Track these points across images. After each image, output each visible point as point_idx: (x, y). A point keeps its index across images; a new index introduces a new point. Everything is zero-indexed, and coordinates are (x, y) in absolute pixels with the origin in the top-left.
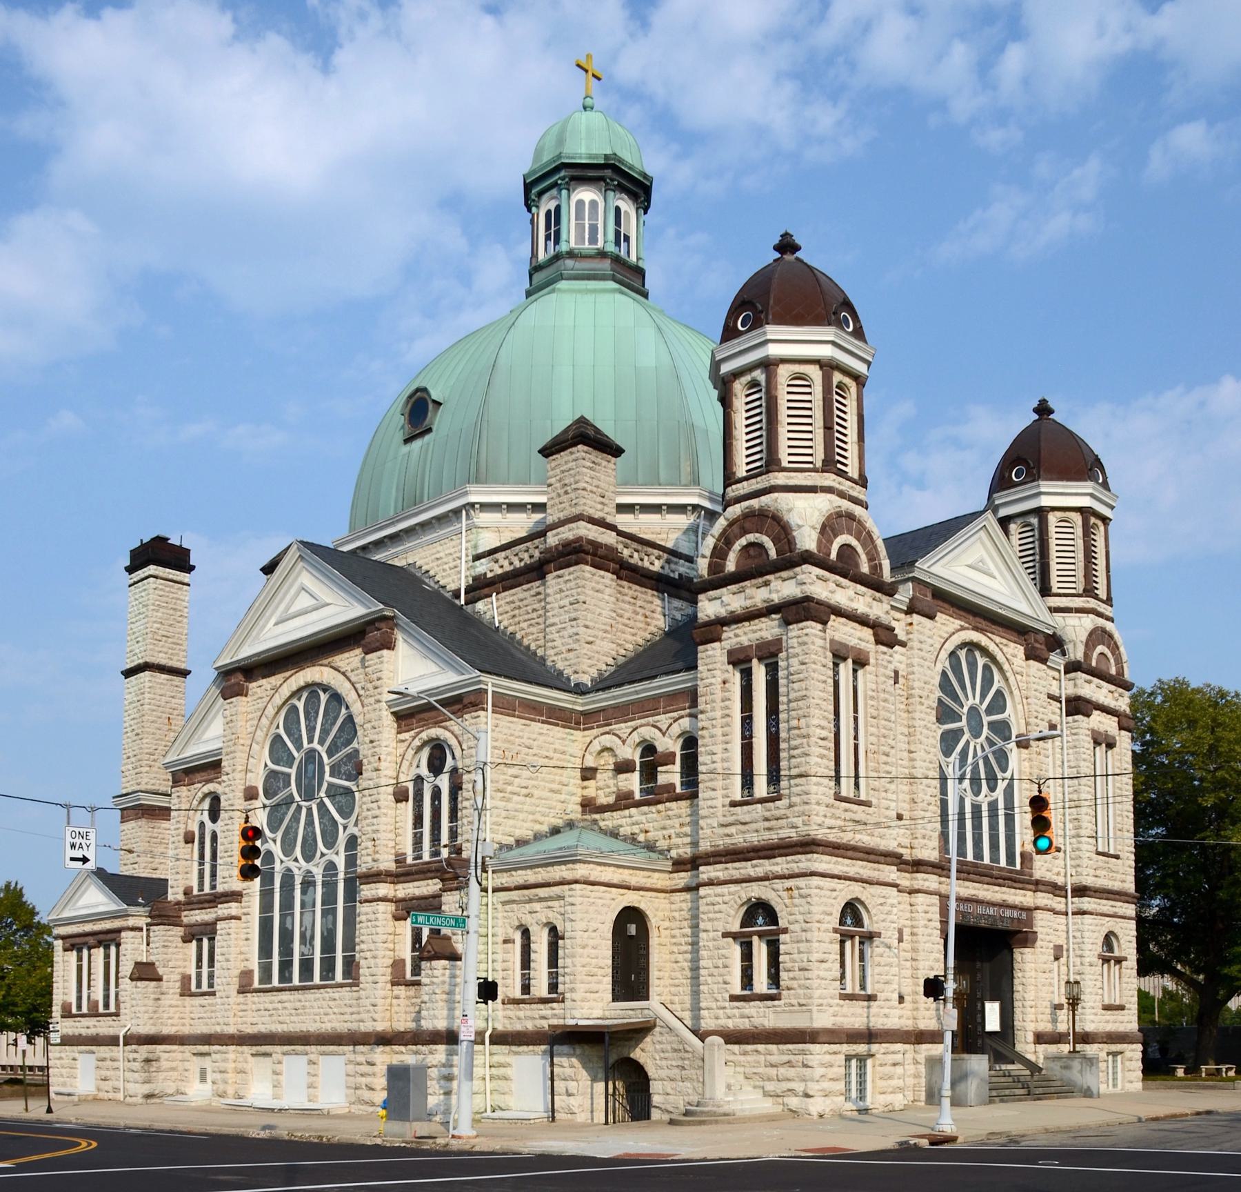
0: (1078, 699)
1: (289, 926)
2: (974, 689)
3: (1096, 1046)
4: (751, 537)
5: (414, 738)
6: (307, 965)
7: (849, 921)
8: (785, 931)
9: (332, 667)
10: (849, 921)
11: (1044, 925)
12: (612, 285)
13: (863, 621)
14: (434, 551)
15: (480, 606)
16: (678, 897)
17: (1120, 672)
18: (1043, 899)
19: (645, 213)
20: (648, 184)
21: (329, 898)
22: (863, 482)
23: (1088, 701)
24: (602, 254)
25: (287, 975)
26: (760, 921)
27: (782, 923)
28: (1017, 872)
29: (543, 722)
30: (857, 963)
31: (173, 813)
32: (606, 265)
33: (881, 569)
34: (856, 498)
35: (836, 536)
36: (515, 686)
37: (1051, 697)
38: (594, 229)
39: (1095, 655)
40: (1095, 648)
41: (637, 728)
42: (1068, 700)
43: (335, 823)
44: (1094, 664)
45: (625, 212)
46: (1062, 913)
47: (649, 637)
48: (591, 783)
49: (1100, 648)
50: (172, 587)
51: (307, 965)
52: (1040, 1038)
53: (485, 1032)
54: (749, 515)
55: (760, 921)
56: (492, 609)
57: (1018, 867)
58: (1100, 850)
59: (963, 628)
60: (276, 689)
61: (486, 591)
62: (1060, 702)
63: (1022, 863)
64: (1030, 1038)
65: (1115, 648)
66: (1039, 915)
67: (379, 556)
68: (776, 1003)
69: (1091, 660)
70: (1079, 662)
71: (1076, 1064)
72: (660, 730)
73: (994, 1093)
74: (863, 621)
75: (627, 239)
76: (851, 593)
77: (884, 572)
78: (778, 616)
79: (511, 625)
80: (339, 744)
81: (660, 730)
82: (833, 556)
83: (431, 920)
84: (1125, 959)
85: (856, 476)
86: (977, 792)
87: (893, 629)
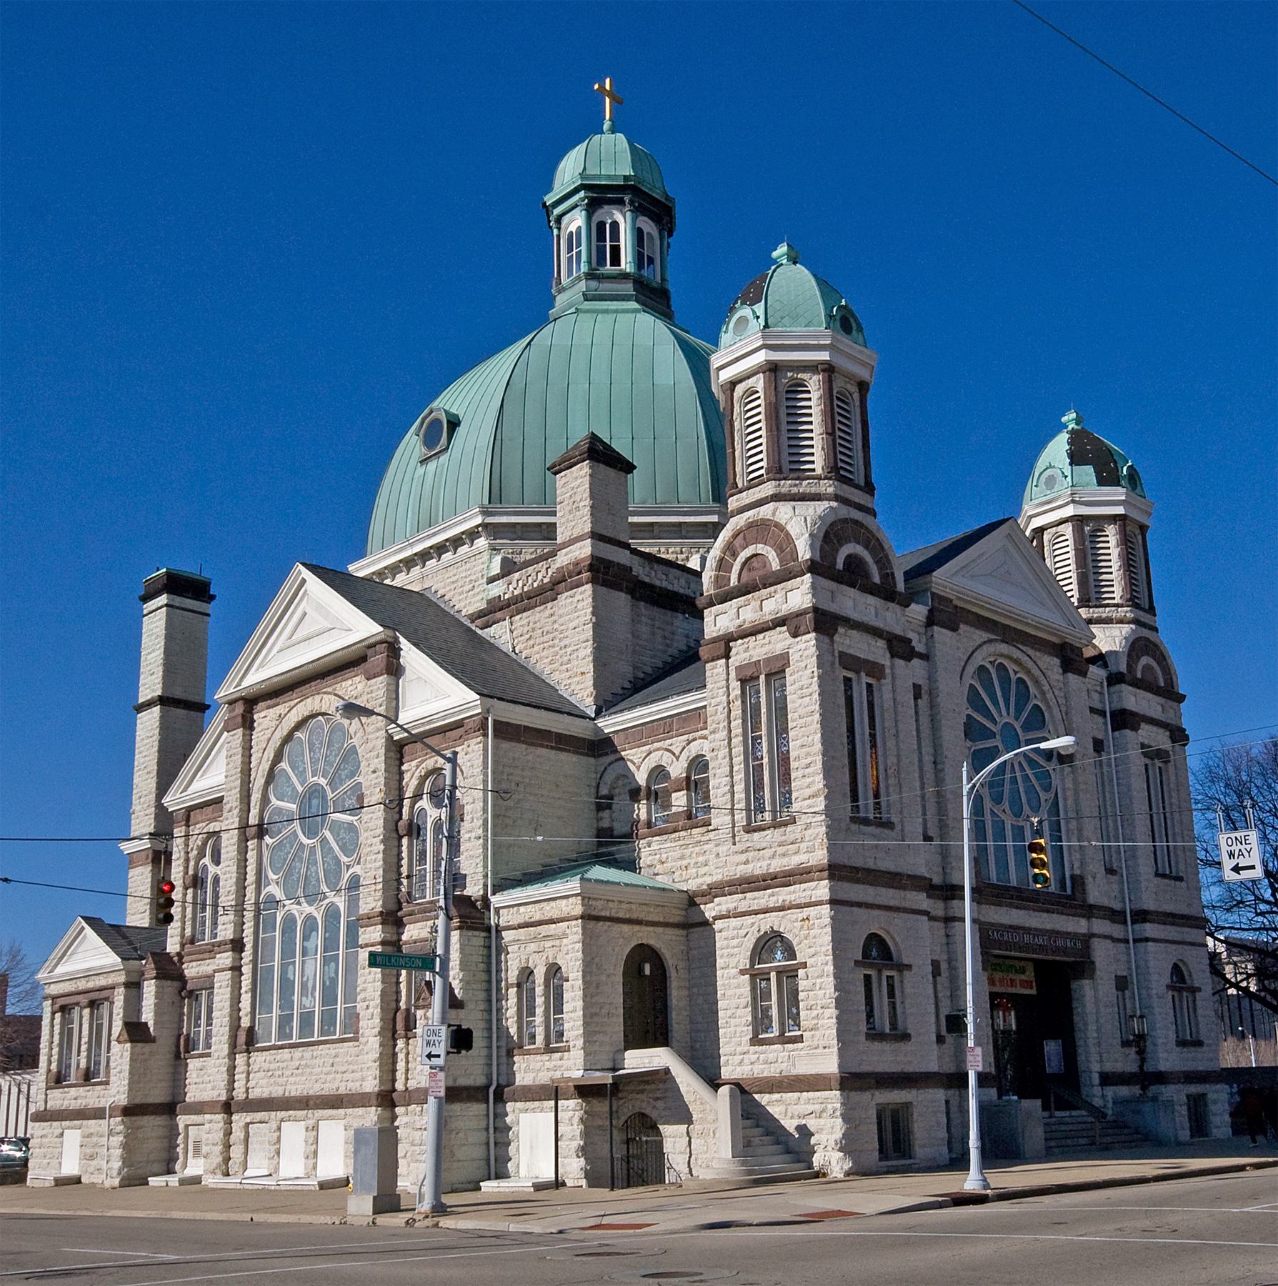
0: (1124, 712)
1: (290, 976)
2: (996, 703)
3: (1172, 1087)
4: (760, 548)
5: (418, 767)
6: (307, 1019)
7: (874, 953)
8: (804, 965)
9: (336, 695)
10: (874, 953)
11: (1102, 953)
12: (635, 305)
13: (875, 632)
14: (451, 574)
15: (491, 631)
16: (669, 931)
17: (1170, 681)
18: (1100, 926)
19: (670, 235)
20: (670, 205)
21: (330, 944)
22: (869, 488)
23: (1133, 714)
24: (624, 276)
25: (288, 1031)
26: (779, 955)
27: (800, 958)
28: (1067, 897)
29: (552, 748)
30: (886, 999)
31: (1078, 872)
32: (628, 288)
33: (893, 578)
34: (859, 504)
35: (841, 545)
36: (629, 716)
37: (1092, 710)
38: (616, 251)
39: (1140, 667)
40: (1139, 658)
41: (650, 753)
42: (1113, 714)
43: (338, 862)
44: (1139, 676)
45: (648, 233)
46: (1119, 941)
47: (669, 660)
48: (606, 814)
49: (1145, 660)
50: (155, 615)
51: (307, 1019)
52: (1107, 1079)
53: (488, 1087)
54: (751, 525)
55: (779, 955)
56: (500, 634)
57: (1069, 891)
58: (1160, 871)
59: (990, 641)
60: (281, 717)
61: (499, 615)
62: (1105, 716)
63: (1073, 888)
64: (1096, 1080)
65: (1162, 659)
66: (1095, 943)
67: (400, 580)
68: (800, 1045)
69: (1135, 671)
70: (1121, 673)
71: (1147, 1108)
72: (674, 754)
73: (1053, 1143)
74: (875, 632)
75: (651, 261)
76: (779, 596)
77: (898, 582)
78: (785, 628)
79: (525, 648)
80: (343, 777)
81: (674, 754)
82: (840, 565)
83: (393, 961)
84: (1199, 989)
85: (862, 483)
86: (1018, 813)
87: (910, 641)
